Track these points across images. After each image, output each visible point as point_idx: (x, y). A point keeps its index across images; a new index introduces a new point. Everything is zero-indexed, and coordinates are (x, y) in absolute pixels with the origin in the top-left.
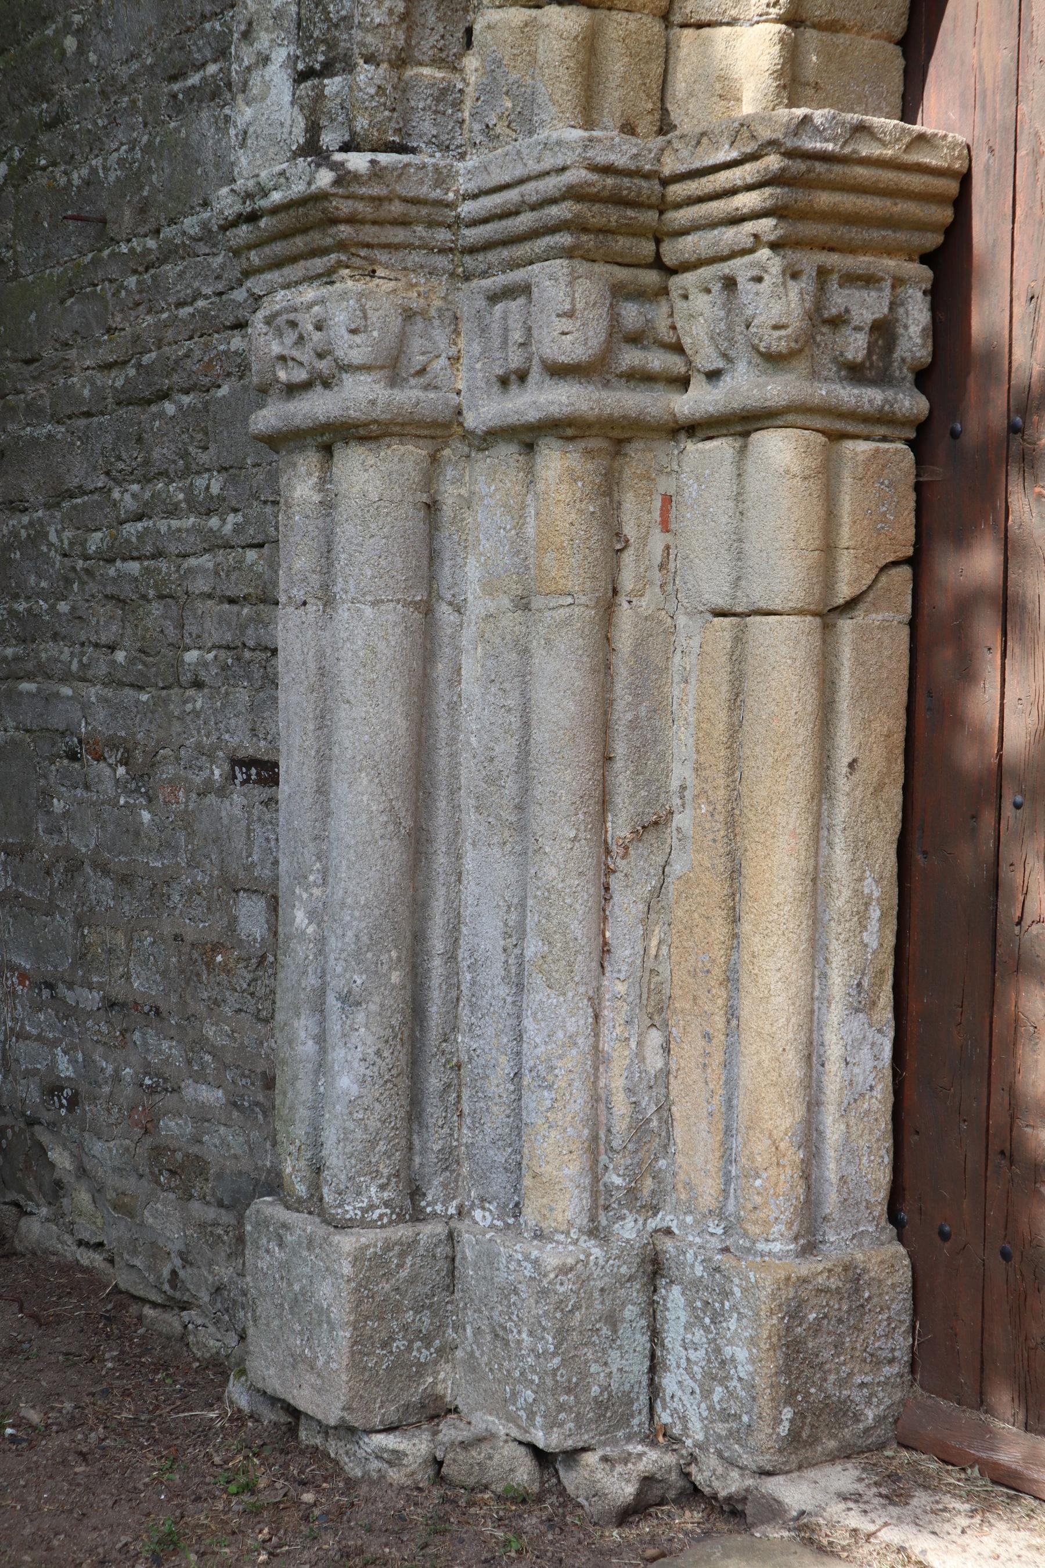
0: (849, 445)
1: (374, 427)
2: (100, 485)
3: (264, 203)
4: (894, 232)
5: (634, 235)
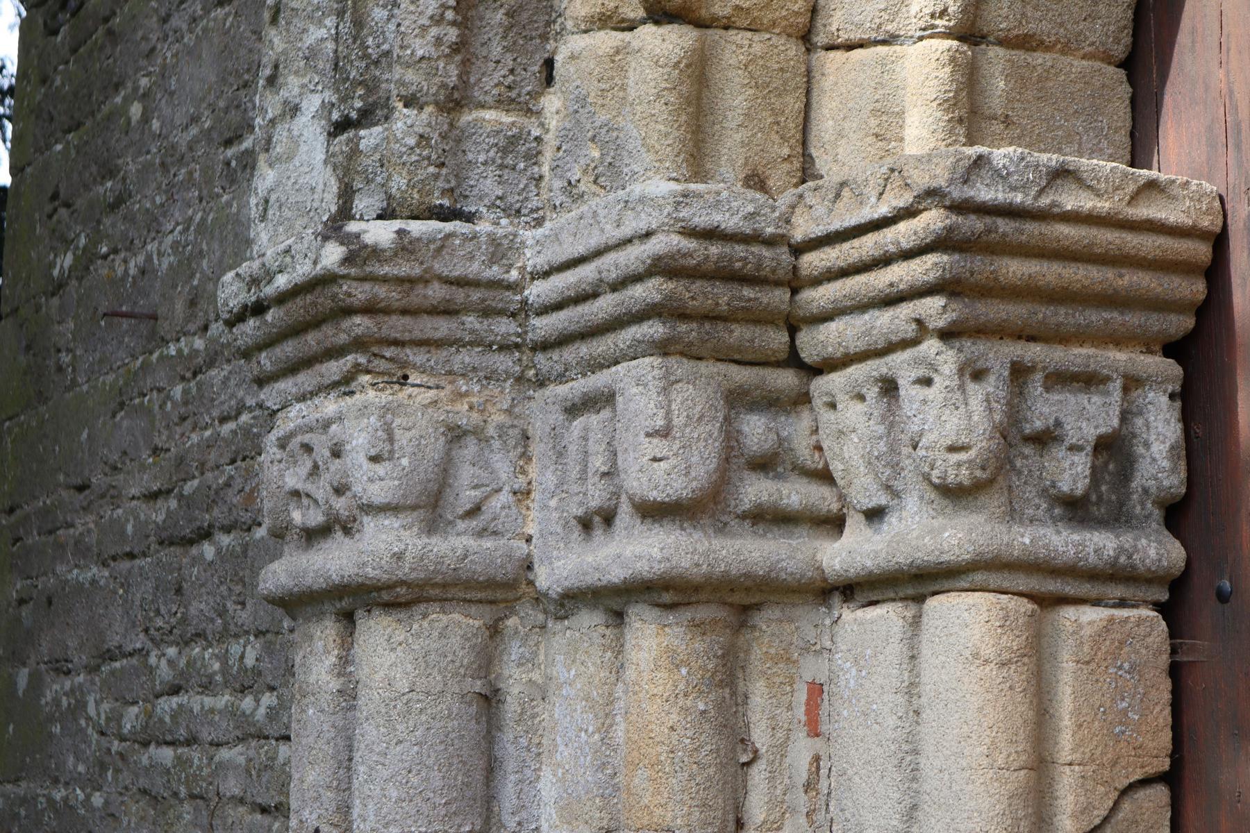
0: (1069, 614)
1: (402, 590)
2: (138, 646)
3: (269, 291)
4: (1122, 314)
5: (757, 322)
